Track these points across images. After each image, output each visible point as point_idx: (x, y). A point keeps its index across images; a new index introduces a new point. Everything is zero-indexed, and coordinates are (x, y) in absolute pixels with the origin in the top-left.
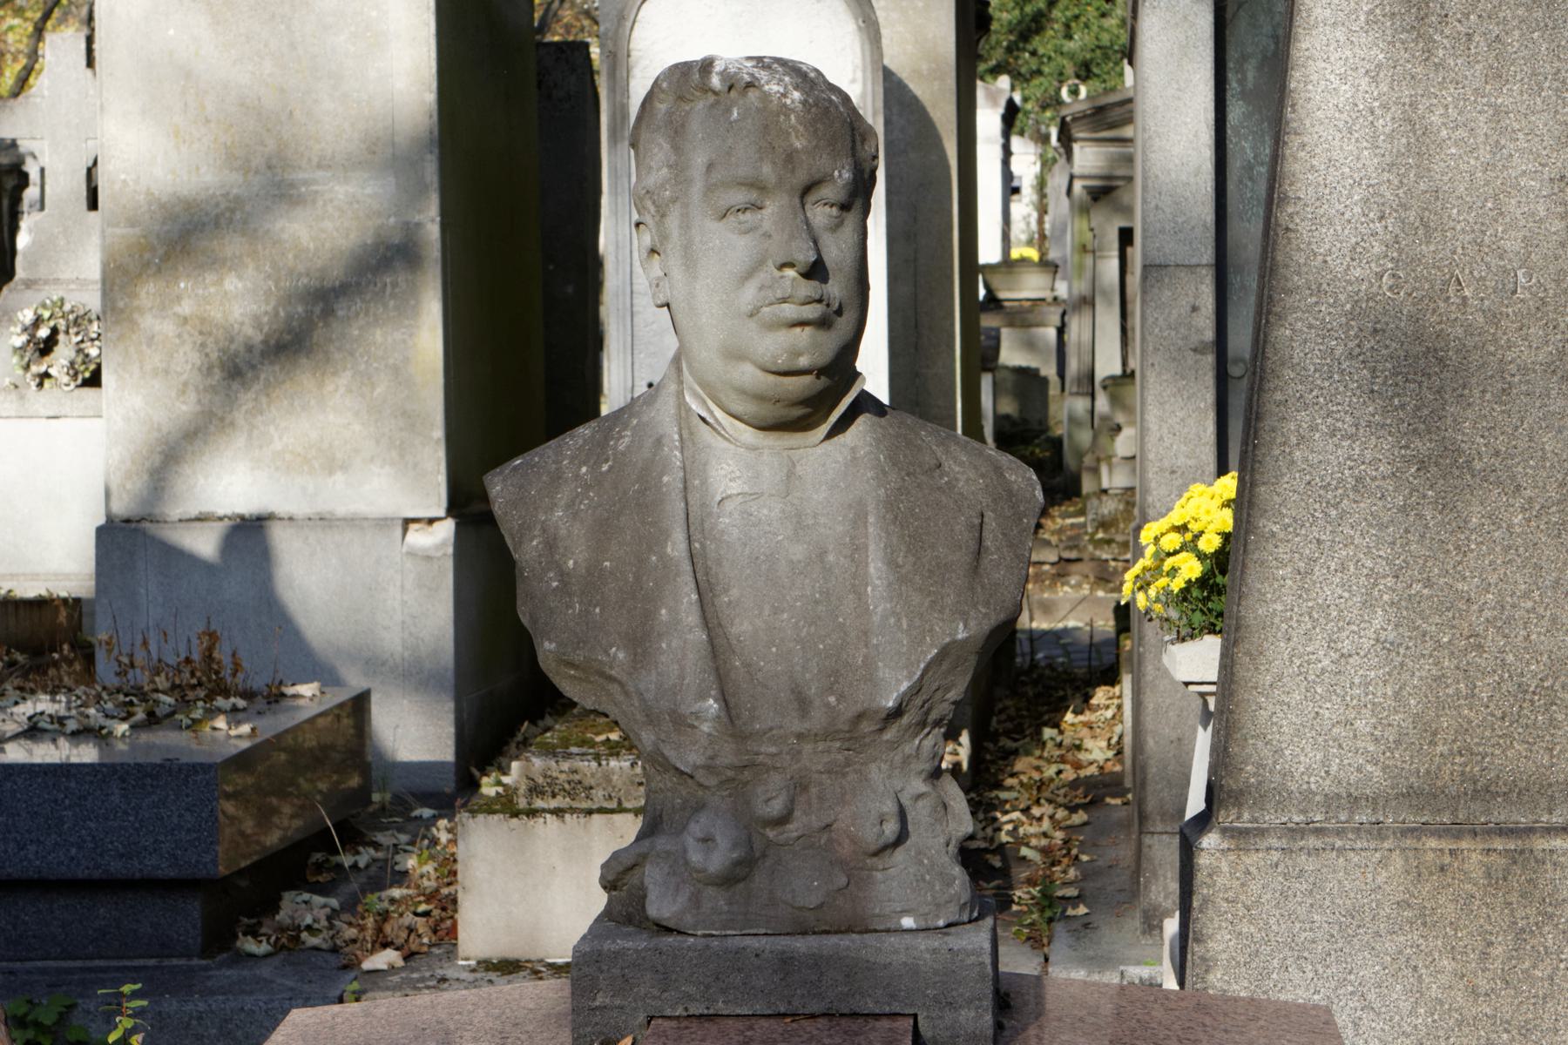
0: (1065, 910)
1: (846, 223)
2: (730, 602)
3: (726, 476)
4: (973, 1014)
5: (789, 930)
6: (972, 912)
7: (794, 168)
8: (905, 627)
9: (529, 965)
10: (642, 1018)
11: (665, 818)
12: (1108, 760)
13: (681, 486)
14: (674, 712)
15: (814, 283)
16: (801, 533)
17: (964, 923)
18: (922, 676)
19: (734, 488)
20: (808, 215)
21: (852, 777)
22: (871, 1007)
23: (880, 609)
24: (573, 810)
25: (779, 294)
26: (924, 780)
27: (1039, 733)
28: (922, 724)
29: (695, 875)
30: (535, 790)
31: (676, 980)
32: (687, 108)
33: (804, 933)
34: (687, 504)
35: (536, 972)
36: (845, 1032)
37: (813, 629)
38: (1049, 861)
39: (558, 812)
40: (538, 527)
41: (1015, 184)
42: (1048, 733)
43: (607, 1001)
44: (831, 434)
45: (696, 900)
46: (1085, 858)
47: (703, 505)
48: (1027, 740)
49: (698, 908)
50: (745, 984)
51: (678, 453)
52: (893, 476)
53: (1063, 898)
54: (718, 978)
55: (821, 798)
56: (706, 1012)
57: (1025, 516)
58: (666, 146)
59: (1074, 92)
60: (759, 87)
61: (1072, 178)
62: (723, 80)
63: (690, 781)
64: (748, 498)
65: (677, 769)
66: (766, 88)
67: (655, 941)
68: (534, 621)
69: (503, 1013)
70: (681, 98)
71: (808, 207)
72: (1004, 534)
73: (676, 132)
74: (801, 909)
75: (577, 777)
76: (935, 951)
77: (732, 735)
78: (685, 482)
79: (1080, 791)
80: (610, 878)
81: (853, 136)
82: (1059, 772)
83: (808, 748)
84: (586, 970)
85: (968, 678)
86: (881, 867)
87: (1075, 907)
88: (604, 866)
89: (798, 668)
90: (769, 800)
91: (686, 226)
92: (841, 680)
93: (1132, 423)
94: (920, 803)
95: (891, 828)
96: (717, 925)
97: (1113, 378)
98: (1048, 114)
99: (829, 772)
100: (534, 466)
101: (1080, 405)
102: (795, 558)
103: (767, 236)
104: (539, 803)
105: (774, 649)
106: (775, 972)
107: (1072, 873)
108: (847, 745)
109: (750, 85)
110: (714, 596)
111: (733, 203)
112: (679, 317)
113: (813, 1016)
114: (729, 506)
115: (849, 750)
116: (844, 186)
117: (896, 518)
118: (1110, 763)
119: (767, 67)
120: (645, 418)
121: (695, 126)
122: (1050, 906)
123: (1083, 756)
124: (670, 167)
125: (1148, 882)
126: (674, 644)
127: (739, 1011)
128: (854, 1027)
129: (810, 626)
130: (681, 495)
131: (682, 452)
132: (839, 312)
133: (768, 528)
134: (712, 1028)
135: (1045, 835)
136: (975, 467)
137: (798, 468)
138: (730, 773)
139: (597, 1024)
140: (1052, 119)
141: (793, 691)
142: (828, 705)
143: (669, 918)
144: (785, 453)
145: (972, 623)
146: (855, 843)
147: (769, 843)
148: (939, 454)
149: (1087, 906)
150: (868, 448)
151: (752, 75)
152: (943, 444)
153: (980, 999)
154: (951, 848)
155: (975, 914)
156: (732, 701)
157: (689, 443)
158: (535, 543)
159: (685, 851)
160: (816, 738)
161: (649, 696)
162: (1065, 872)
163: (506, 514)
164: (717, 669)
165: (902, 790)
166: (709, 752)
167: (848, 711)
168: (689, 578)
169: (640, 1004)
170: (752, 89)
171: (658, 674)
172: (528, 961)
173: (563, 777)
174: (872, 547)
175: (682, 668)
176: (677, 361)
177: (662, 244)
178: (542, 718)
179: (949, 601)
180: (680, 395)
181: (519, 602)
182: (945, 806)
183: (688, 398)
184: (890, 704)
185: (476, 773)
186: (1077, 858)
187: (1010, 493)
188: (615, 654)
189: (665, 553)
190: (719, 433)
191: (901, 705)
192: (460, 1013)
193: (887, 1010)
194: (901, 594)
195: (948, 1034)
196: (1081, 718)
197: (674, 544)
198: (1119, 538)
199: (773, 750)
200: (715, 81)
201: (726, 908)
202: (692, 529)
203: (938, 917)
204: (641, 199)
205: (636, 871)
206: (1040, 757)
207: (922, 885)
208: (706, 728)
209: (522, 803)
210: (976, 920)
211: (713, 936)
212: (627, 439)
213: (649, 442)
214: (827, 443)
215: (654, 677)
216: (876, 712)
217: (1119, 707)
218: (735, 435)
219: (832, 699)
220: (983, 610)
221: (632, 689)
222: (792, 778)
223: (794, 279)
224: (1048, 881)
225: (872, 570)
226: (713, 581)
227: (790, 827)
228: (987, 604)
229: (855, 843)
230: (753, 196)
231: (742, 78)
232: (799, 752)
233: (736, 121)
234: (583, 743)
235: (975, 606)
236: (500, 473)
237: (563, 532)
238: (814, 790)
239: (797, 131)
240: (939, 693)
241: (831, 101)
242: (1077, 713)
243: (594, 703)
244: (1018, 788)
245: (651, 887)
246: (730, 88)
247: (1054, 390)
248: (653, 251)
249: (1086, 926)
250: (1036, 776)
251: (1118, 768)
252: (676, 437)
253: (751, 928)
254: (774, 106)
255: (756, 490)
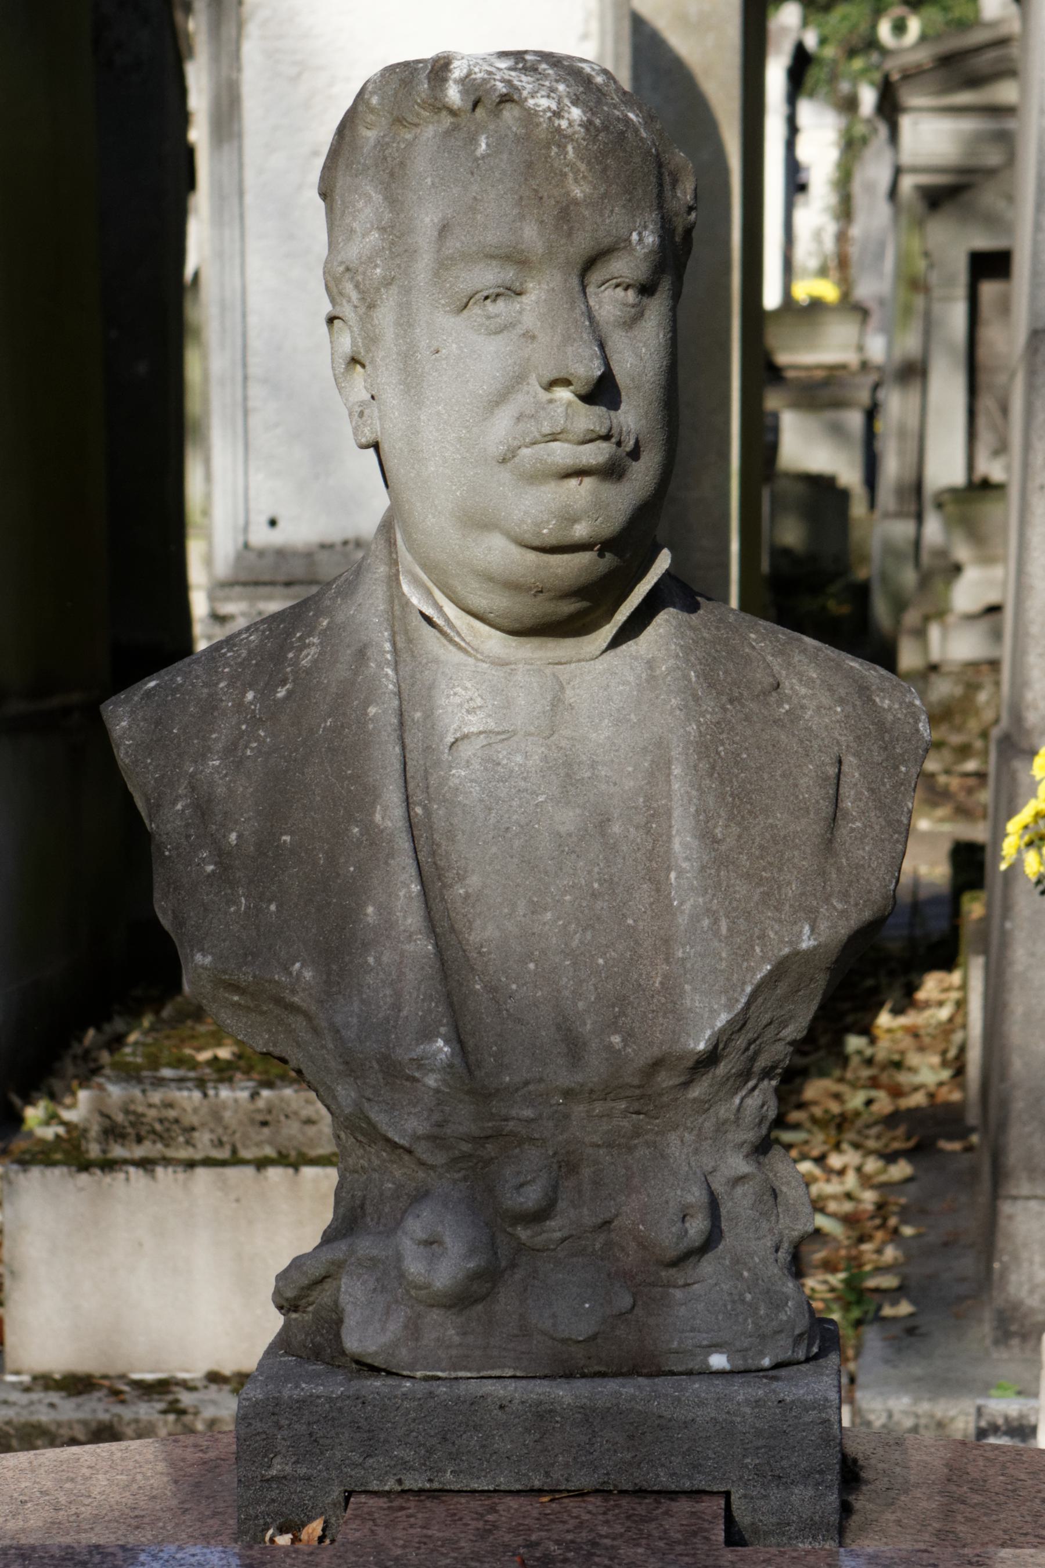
0: (879, 1308)
1: (647, 313)
2: (467, 896)
3: (461, 705)
4: (811, 1492)
5: (547, 1372)
6: (810, 1346)
7: (571, 229)
8: (724, 930)
9: (106, 1383)
10: (336, 1493)
11: (369, 1209)
12: (941, 1084)
13: (395, 721)
14: (386, 1057)
15: (600, 410)
16: (573, 791)
17: (799, 1363)
18: (748, 1004)
19: (474, 723)
20: (592, 303)
21: (642, 1152)
22: (664, 1480)
23: (687, 907)
24: (166, 1161)
25: (546, 429)
26: (747, 1156)
27: (838, 1043)
28: (745, 1075)
29: (413, 1292)
30: (112, 1132)
31: (386, 1441)
32: (408, 136)
33: (569, 1376)
34: (403, 747)
35: (115, 1393)
36: (628, 1517)
37: (589, 935)
38: (855, 1234)
39: (146, 1164)
40: (185, 783)
41: (803, 177)
42: (854, 1043)
43: (288, 1469)
44: (616, 642)
45: (414, 1329)
46: (908, 1231)
47: (428, 749)
48: (822, 1053)
49: (417, 1340)
50: (483, 1446)
51: (389, 671)
52: (709, 704)
53: (877, 1290)
54: (445, 1439)
55: (597, 1183)
56: (428, 1486)
57: (904, 762)
58: (377, 198)
59: (900, 28)
60: (520, 103)
61: (898, 171)
62: (464, 93)
63: (406, 1157)
64: (494, 739)
65: (388, 1140)
66: (531, 102)
67: (356, 1384)
68: (180, 922)
69: (134, 1480)
70: (399, 121)
71: (590, 290)
72: (872, 790)
73: (392, 174)
74: (564, 1341)
75: (172, 1114)
76: (758, 1403)
77: (470, 1092)
78: (401, 715)
79: (901, 1131)
80: (290, 1294)
81: (660, 177)
82: (869, 1102)
83: (579, 1110)
84: (258, 1425)
85: (814, 1006)
86: (681, 1282)
87: (895, 1303)
88: (279, 1278)
89: (566, 993)
90: (522, 1185)
91: (406, 322)
92: (629, 1010)
93: (987, 560)
94: (739, 1190)
95: (697, 1227)
96: (444, 1364)
97: (953, 491)
98: (858, 64)
99: (609, 1145)
100: (175, 691)
101: (902, 530)
102: (563, 830)
103: (530, 336)
104: (118, 1151)
105: (532, 966)
106: (527, 1430)
107: (890, 1253)
108: (636, 1106)
109: (505, 99)
110: (444, 886)
111: (480, 286)
112: (390, 464)
113: (581, 1494)
114: (466, 750)
115: (638, 1113)
116: (646, 255)
117: (713, 768)
118: (944, 1090)
119: (531, 69)
120: (340, 618)
121: (421, 164)
122: (859, 1302)
123: (904, 1078)
124: (382, 230)
125: (1005, 1269)
126: (385, 959)
127: (475, 1486)
128: (641, 1510)
129: (584, 930)
130: (394, 736)
131: (396, 670)
132: (635, 454)
133: (523, 784)
134: (438, 1509)
135: (849, 1196)
136: (831, 689)
137: (569, 692)
138: (466, 1147)
139: (273, 1501)
140: (865, 72)
141: (559, 1028)
142: (610, 1047)
143: (376, 1353)
144: (549, 670)
145: (823, 926)
146: (645, 1248)
147: (521, 1248)
148: (776, 668)
149: (913, 1301)
150: (671, 662)
151: (509, 83)
152: (782, 653)
153: (821, 1472)
154: (781, 1254)
155: (815, 1350)
156: (471, 1043)
157: (405, 656)
158: (179, 807)
159: (399, 1258)
160: (592, 1095)
161: (350, 1034)
162: (879, 1251)
163: (136, 762)
164: (449, 995)
165: (715, 1170)
166: (436, 1117)
167: (640, 1056)
168: (409, 861)
169: (334, 1473)
170: (508, 105)
171: (363, 1001)
172: (105, 1377)
173: (152, 1113)
174: (677, 813)
175: (398, 994)
176: (387, 527)
177: (368, 350)
178: (109, 1019)
179: (791, 890)
180: (393, 581)
181: (157, 895)
182: (775, 1194)
183: (406, 588)
184: (701, 1046)
185: (17, 1101)
186: (896, 1231)
187: (882, 727)
188: (299, 973)
189: (372, 822)
190: (451, 641)
191: (716, 1046)
192: (72, 1480)
193: (687, 1485)
194: (719, 883)
195: (774, 1520)
196: (903, 1020)
197: (385, 809)
198: (956, 739)
199: (528, 1113)
200: (453, 94)
201: (457, 1339)
202: (411, 786)
203: (762, 1354)
204: (338, 281)
205: (327, 1285)
206: (841, 1080)
207: (740, 1307)
208: (431, 1081)
209: (94, 1151)
210: (816, 1357)
211: (439, 1378)
212: (313, 650)
213: (347, 655)
214: (611, 653)
215: (356, 1006)
216: (680, 1058)
217: (961, 1005)
218: (475, 643)
219: (616, 1039)
220: (839, 906)
221: (324, 1024)
222: (555, 1154)
223: (569, 404)
224: (855, 1262)
225: (677, 846)
226: (441, 863)
227: (552, 1224)
228: (845, 896)
229: (645, 1248)
230: (509, 274)
231: (494, 88)
232: (567, 1116)
233: (483, 157)
234: (180, 1062)
235: (827, 900)
236: (128, 700)
237: (221, 791)
238: (586, 1172)
239: (576, 172)
240: (772, 1030)
241: (627, 121)
242: (897, 1011)
243: (266, 1044)
244: (808, 1124)
245: (349, 1308)
246: (475, 105)
247: (858, 509)
248: (354, 361)
249: (911, 1331)
250: (835, 1108)
251: (956, 1096)
252: (388, 646)
253: (493, 1368)
254: (541, 132)
255: (506, 726)
